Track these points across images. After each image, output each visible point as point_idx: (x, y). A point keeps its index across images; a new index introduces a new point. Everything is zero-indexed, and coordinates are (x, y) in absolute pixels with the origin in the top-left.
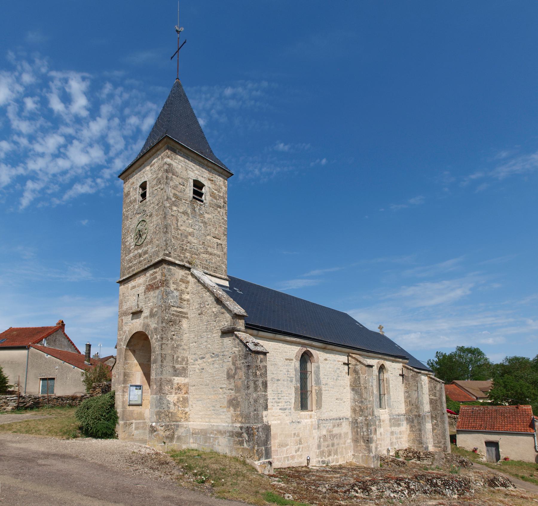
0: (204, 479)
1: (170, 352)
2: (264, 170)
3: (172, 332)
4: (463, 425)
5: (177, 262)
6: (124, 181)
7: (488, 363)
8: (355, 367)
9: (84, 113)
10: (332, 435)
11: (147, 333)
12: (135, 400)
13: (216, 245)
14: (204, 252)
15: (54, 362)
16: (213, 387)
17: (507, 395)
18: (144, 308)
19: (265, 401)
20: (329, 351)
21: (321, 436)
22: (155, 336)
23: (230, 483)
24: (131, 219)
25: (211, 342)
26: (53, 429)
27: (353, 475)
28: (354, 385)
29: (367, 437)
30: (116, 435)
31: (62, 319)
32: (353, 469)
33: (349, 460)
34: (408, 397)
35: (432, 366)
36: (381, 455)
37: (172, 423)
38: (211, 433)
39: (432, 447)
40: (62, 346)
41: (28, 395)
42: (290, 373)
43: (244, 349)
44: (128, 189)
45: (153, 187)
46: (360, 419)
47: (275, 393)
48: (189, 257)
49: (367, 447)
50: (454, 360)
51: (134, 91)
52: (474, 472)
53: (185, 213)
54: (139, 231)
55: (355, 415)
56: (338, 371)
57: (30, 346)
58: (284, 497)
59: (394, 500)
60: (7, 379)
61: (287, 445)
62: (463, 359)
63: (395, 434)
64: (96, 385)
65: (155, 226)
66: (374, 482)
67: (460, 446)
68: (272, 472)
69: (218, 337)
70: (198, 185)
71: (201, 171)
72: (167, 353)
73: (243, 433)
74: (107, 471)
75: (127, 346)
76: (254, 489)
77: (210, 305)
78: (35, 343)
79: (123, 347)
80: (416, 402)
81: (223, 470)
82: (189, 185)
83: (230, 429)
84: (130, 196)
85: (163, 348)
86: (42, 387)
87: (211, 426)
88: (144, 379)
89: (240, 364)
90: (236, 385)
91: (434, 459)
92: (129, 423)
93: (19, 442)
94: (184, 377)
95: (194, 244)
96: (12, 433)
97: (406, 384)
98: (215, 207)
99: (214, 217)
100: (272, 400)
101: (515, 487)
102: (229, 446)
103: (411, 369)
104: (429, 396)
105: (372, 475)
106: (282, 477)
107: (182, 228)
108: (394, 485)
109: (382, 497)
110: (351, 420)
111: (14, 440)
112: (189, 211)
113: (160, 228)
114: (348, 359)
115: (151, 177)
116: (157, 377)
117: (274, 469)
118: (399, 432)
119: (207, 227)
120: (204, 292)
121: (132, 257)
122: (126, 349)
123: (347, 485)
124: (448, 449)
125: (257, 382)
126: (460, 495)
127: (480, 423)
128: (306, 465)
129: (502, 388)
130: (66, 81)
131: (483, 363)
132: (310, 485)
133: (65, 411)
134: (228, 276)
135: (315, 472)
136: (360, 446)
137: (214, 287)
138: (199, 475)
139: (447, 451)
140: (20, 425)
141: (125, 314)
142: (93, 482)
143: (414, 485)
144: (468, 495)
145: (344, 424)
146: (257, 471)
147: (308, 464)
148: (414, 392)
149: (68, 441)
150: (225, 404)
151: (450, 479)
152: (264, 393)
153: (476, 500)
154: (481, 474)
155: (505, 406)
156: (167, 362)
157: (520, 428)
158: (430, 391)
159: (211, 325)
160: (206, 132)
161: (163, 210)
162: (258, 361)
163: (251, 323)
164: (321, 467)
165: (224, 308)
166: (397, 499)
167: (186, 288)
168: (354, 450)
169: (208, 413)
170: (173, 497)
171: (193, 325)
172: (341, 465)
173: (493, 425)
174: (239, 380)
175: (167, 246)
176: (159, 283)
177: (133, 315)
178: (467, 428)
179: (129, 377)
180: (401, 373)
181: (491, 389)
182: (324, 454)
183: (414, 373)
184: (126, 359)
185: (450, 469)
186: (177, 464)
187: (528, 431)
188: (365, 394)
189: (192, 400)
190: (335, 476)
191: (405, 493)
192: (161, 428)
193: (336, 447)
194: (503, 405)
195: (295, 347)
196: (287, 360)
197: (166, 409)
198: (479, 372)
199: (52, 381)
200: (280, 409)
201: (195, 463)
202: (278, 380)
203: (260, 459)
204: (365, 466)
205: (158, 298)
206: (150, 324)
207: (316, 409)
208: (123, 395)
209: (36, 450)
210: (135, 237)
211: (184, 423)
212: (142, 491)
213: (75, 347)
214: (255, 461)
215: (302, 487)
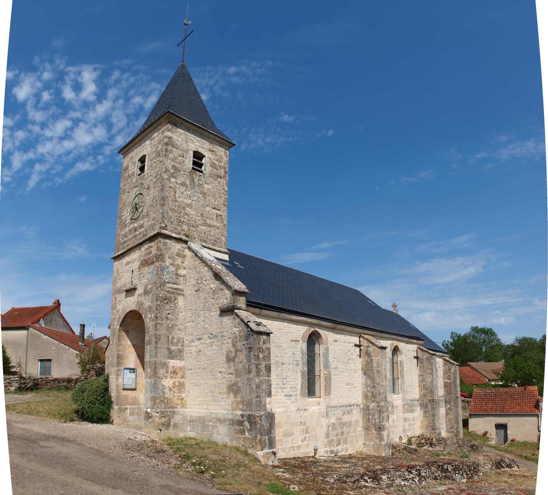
0: (204, 469)
1: (164, 332)
2: (268, 140)
3: (167, 310)
4: (476, 409)
5: (174, 235)
7: (501, 344)
8: (367, 349)
9: (92, 98)
10: (342, 423)
11: (140, 312)
12: (129, 384)
13: (215, 216)
14: (202, 224)
15: (51, 343)
16: (211, 372)
17: (517, 377)
18: (138, 285)
19: (269, 386)
21: (329, 425)
23: (232, 475)
24: (128, 193)
25: (209, 321)
26: (51, 412)
27: (363, 464)
28: (366, 369)
29: (379, 424)
31: (58, 298)
32: (363, 458)
33: (359, 449)
34: (422, 380)
35: (447, 347)
36: (393, 443)
37: (168, 410)
38: (210, 421)
39: (445, 433)
40: (58, 327)
43: (245, 329)
45: (152, 161)
46: (372, 405)
47: (280, 377)
48: (186, 230)
49: (379, 435)
50: (468, 340)
51: (140, 75)
52: (483, 455)
53: (183, 184)
54: (136, 204)
55: (367, 402)
56: (349, 354)
57: (29, 326)
58: (289, 488)
59: (404, 488)
60: (10, 359)
61: (293, 434)
62: (477, 340)
63: (408, 420)
65: (152, 199)
66: (385, 471)
67: (472, 430)
68: (276, 463)
70: (198, 157)
71: (201, 143)
72: (161, 334)
73: (244, 421)
74: (104, 456)
75: (121, 326)
76: (257, 480)
79: (117, 327)
80: (431, 387)
81: (223, 461)
82: (188, 156)
83: (230, 417)
84: (129, 170)
85: (158, 328)
86: (40, 369)
87: (209, 413)
88: (138, 361)
89: (240, 346)
91: (446, 445)
93: (22, 423)
94: (179, 360)
95: (192, 216)
96: (16, 414)
97: (421, 367)
98: (215, 178)
99: (213, 187)
100: (276, 386)
101: (519, 468)
102: (229, 435)
103: (425, 351)
104: (444, 379)
105: (383, 463)
106: (287, 467)
107: (179, 200)
108: (405, 473)
109: (392, 486)
110: (362, 407)
111: (18, 420)
112: (188, 182)
113: (157, 201)
114: (360, 340)
115: (150, 150)
116: (151, 360)
117: (279, 459)
118: (412, 418)
119: (206, 198)
120: (202, 267)
123: (357, 475)
124: (460, 434)
126: (469, 479)
127: (492, 406)
128: (313, 455)
129: (512, 370)
130: (79, 73)
131: (495, 344)
132: (317, 476)
133: (62, 393)
134: (228, 249)
135: (322, 462)
136: (371, 434)
137: (213, 261)
138: (197, 464)
139: (459, 436)
140: (22, 406)
141: (119, 291)
142: (91, 467)
143: (425, 472)
144: (476, 478)
145: (354, 411)
146: (260, 462)
147: (315, 454)
148: (428, 375)
149: (65, 424)
150: (225, 390)
151: (460, 464)
152: (267, 378)
153: (483, 482)
154: (489, 457)
155: (514, 388)
156: (162, 344)
157: (526, 409)
158: (445, 374)
159: (209, 302)
161: (161, 182)
162: (260, 343)
163: (253, 300)
164: (330, 457)
166: (407, 486)
167: (183, 263)
168: (365, 439)
170: (171, 486)
171: (190, 302)
173: (503, 408)
175: (164, 219)
177: (126, 293)
178: (479, 412)
179: (122, 359)
180: (415, 355)
181: (502, 371)
182: (333, 443)
183: (429, 355)
184: (119, 340)
185: (461, 454)
186: (174, 453)
187: (533, 412)
188: (378, 379)
190: (344, 466)
191: (416, 480)
192: (157, 414)
193: (345, 436)
194: (512, 387)
195: (301, 327)
196: (292, 341)
198: (492, 354)
199: (49, 362)
200: (285, 396)
201: (193, 452)
202: (283, 364)
203: (263, 449)
204: (376, 454)
205: (153, 273)
206: (145, 302)
208: (117, 379)
211: (181, 410)
213: (70, 327)
214: (258, 451)
215: (308, 478)
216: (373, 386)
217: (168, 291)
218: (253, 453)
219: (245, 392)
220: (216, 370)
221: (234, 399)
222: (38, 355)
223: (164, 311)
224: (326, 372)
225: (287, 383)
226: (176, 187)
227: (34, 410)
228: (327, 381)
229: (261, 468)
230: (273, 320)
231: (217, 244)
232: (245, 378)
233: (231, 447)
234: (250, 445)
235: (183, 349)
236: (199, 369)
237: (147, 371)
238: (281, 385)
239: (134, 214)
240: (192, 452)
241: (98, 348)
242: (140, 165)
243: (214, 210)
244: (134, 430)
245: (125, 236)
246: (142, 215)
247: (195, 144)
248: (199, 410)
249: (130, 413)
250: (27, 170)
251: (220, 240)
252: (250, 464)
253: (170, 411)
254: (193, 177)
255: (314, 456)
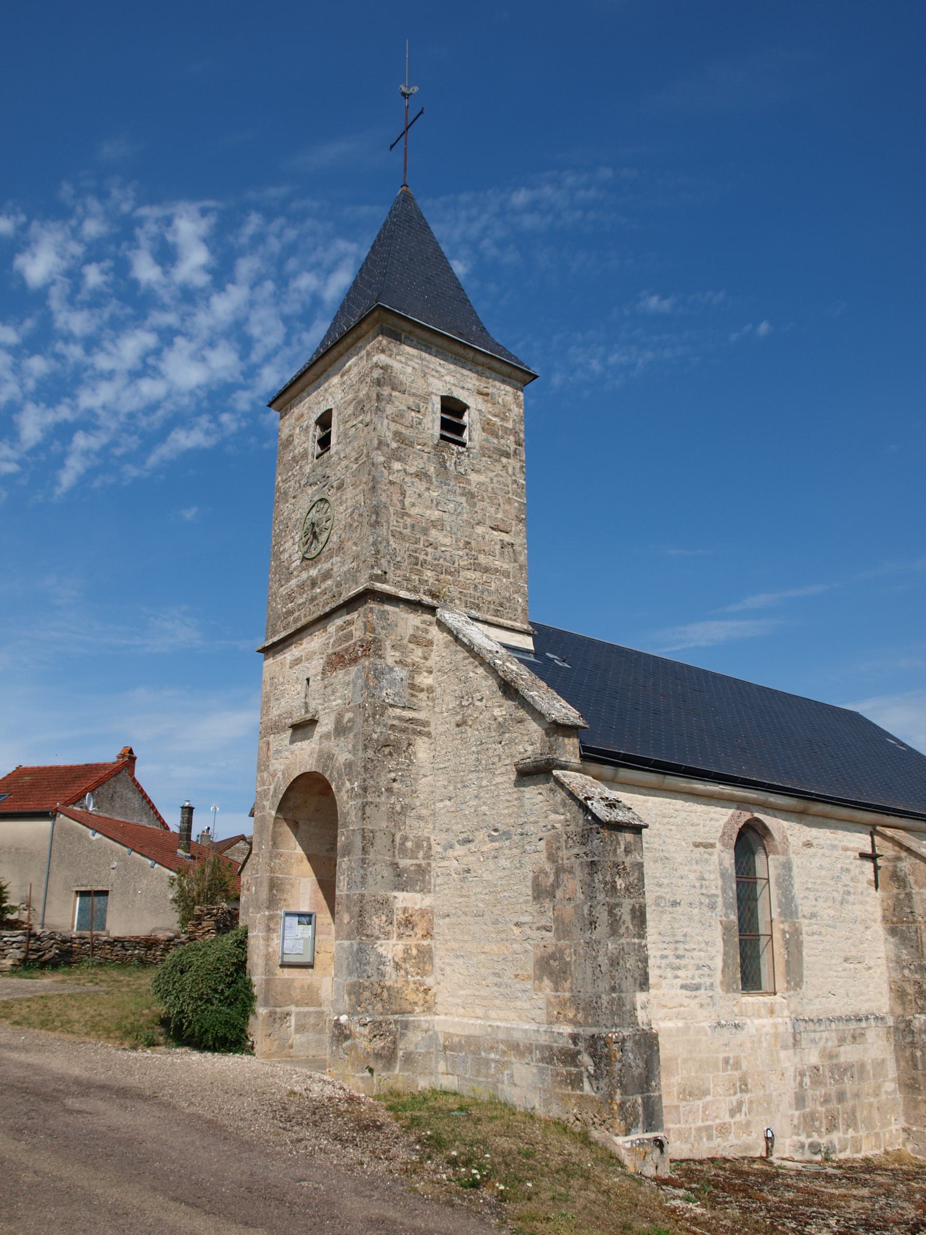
0: (478, 1177)
1: (384, 824)
2: (613, 359)
3: (390, 771)
5: (403, 594)
6: (281, 414)
8: (895, 866)
9: (202, 280)
10: (838, 1066)
11: (327, 776)
13: (498, 547)
14: (469, 567)
15: (109, 852)
16: (496, 922)
18: (322, 713)
20: (816, 819)
22: (348, 784)
23: (550, 1194)
24: (294, 498)
25: (490, 798)
26: (100, 1021)
28: (895, 919)
30: (250, 1043)
31: (130, 745)
33: (891, 1144)
38: (492, 1048)
40: (129, 812)
41: (48, 933)
42: (707, 883)
43: (580, 816)
44: (290, 431)
45: (346, 422)
48: (431, 581)
51: (310, 223)
53: (421, 475)
54: (313, 524)
55: (904, 1009)
56: (846, 878)
57: (57, 810)
60: (5, 890)
61: (706, 1093)
64: (202, 911)
65: (349, 511)
68: (665, 1172)
69: (507, 785)
71: (458, 376)
72: (377, 828)
73: (579, 1052)
74: (225, 1139)
75: (280, 809)
76: (618, 1218)
77: (487, 701)
78: (69, 804)
79: (269, 814)
81: (528, 1155)
83: (543, 1040)
84: (294, 446)
85: (368, 814)
87: (489, 1029)
88: (320, 895)
89: (568, 859)
90: (558, 916)
92: (282, 1013)
93: (25, 1049)
95: (443, 549)
96: (11, 1026)
98: (494, 456)
99: (492, 479)
100: (658, 962)
102: (540, 1089)
106: (694, 1186)
107: (414, 511)
110: (891, 1024)
111: (14, 1042)
112: (432, 470)
114: (873, 842)
115: (342, 399)
116: (352, 892)
117: (671, 1161)
119: (475, 504)
120: (471, 667)
121: (295, 589)
122: (276, 818)
125: (617, 909)
128: (764, 1155)
130: (168, 221)
132: (780, 1217)
133: (130, 975)
134: (531, 623)
137: (497, 652)
140: (29, 1007)
141: (275, 728)
142: (192, 1167)
145: (871, 1035)
146: (623, 1166)
147: (769, 1150)
149: (134, 1054)
150: (530, 969)
152: (636, 941)
159: (490, 753)
160: (471, 289)
161: (370, 471)
162: (618, 852)
165: (522, 707)
167: (426, 658)
169: (482, 993)
170: (394, 1222)
171: (444, 752)
172: (870, 1160)
174: (566, 902)
175: (379, 557)
176: (357, 648)
182: (817, 1124)
184: (275, 844)
186: (405, 1132)
189: (442, 953)
190: (855, 1192)
192: (362, 1029)
193: (850, 1103)
196: (697, 845)
197: (374, 979)
199: (102, 898)
200: (682, 987)
201: (453, 1130)
202: (675, 904)
203: (630, 1130)
205: (355, 685)
206: (336, 753)
207: (787, 989)
209: (61, 1071)
210: (304, 539)
211: (422, 1019)
212: (314, 1198)
213: (156, 812)
214: (617, 1135)
215: (757, 1222)
216: (920, 965)
217: (393, 725)
218: (604, 1140)
219: (580, 977)
220: (507, 919)
221: (553, 993)
222: (76, 881)
223: (384, 773)
224: (786, 927)
225: (688, 954)
226: (406, 483)
227: (58, 1016)
228: (790, 949)
229: (627, 1182)
230: (647, 792)
231: (506, 611)
232: (582, 941)
233: (546, 1121)
234: (595, 1116)
235: (429, 864)
236: (466, 915)
237: (341, 921)
238: (672, 959)
239: (309, 548)
240: (449, 1129)
241: (223, 865)
242: (318, 433)
243: (494, 532)
244: (304, 1070)
245: (290, 598)
246: (327, 548)
247: (445, 381)
248: (465, 1020)
249: (296, 1025)
250: (56, 447)
251: (513, 601)
252: (597, 1171)
253: (396, 1022)
254: (444, 456)
255: (767, 1157)
